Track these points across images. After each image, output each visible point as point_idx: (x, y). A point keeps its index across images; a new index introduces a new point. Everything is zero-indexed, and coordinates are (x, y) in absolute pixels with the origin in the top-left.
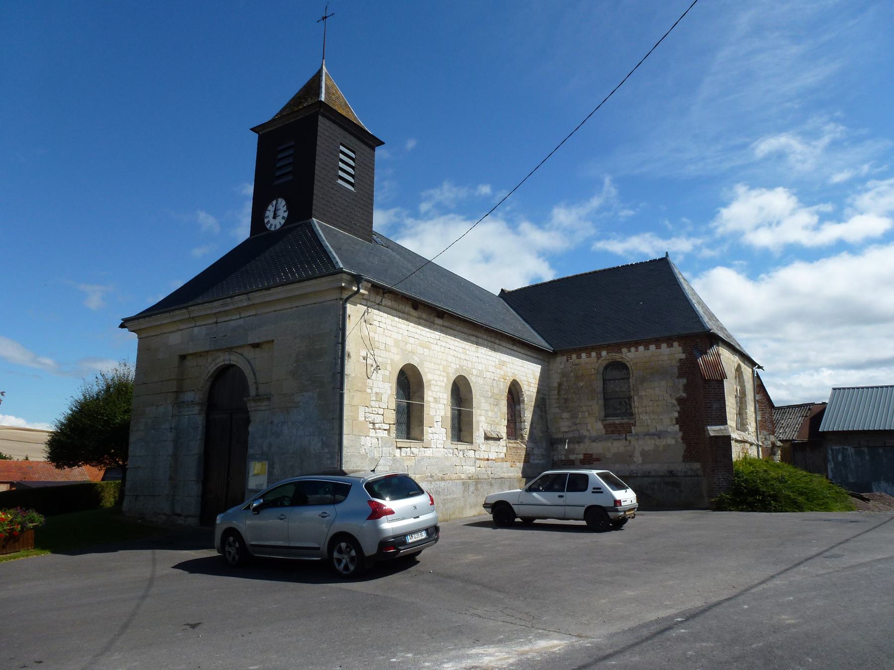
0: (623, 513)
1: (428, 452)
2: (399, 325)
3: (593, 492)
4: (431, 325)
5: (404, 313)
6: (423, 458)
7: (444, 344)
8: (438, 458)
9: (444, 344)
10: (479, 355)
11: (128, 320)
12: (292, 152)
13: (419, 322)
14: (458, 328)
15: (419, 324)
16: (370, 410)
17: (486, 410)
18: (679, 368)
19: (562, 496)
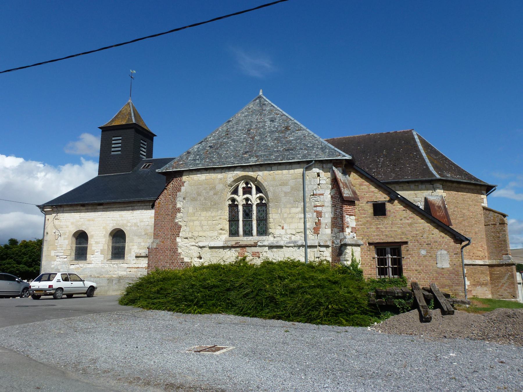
0: (32, 292)
1: (90, 266)
2: (89, 215)
3: (57, 282)
4: (95, 210)
5: (77, 210)
6: (86, 268)
7: (105, 216)
8: (96, 268)
9: (105, 216)
10: (133, 215)
11: (413, 208)
12: (112, 153)
13: (87, 211)
14: (115, 206)
15: (88, 212)
16: (57, 251)
17: (139, 243)
18: (180, 190)
19: (72, 283)
